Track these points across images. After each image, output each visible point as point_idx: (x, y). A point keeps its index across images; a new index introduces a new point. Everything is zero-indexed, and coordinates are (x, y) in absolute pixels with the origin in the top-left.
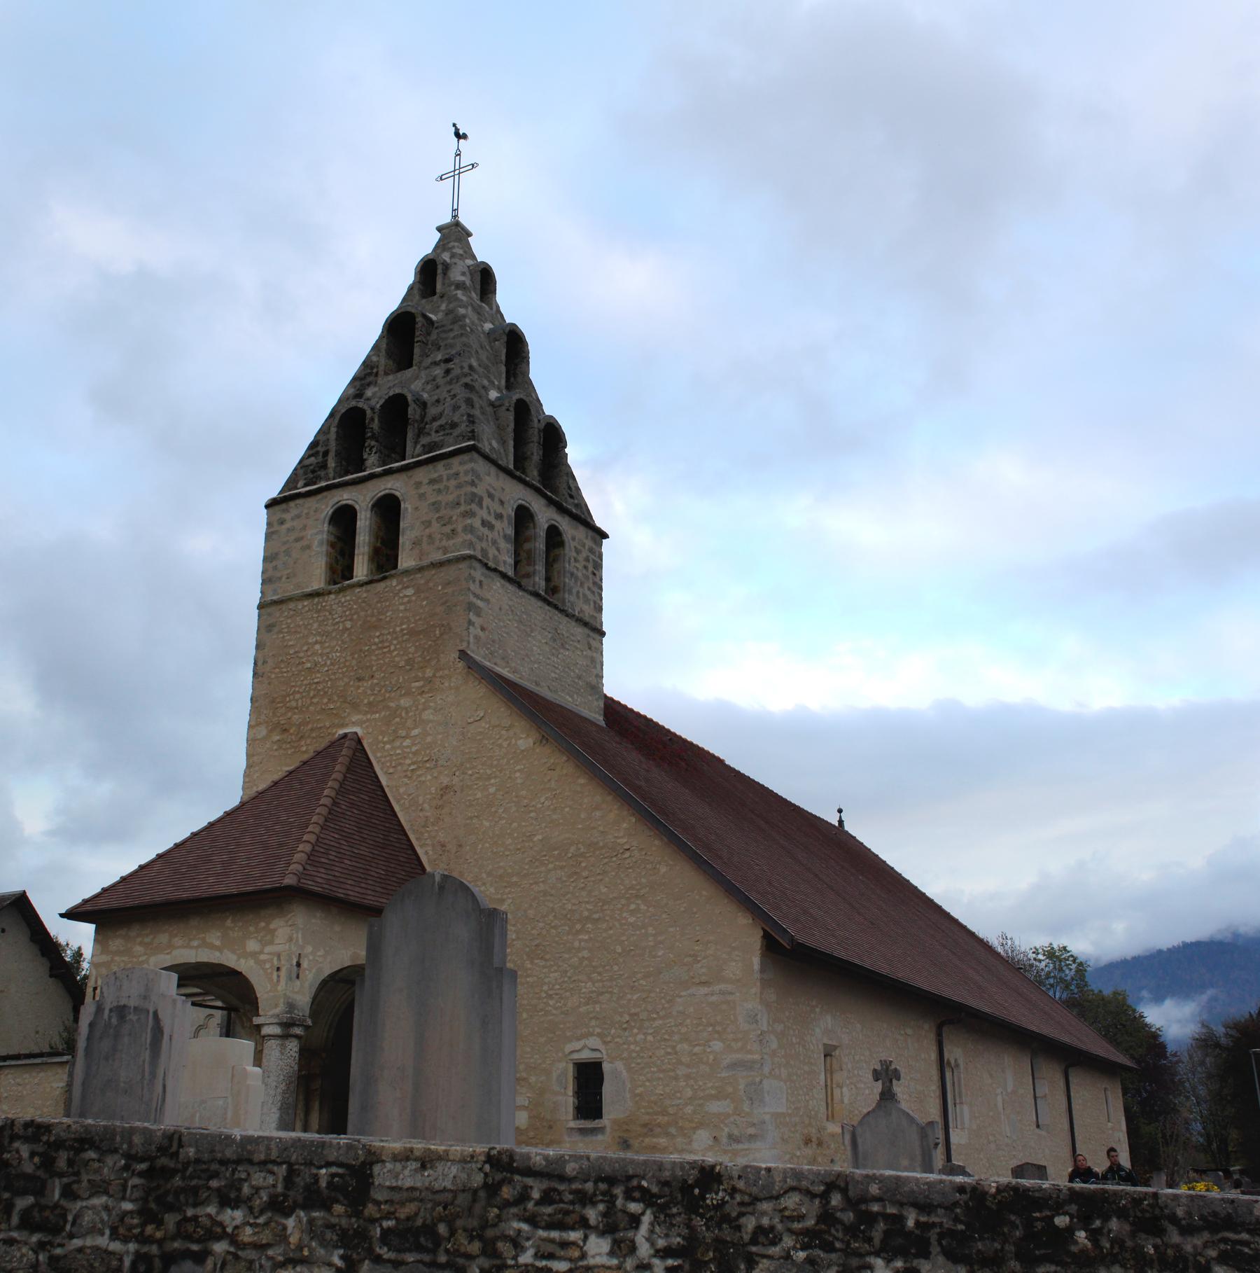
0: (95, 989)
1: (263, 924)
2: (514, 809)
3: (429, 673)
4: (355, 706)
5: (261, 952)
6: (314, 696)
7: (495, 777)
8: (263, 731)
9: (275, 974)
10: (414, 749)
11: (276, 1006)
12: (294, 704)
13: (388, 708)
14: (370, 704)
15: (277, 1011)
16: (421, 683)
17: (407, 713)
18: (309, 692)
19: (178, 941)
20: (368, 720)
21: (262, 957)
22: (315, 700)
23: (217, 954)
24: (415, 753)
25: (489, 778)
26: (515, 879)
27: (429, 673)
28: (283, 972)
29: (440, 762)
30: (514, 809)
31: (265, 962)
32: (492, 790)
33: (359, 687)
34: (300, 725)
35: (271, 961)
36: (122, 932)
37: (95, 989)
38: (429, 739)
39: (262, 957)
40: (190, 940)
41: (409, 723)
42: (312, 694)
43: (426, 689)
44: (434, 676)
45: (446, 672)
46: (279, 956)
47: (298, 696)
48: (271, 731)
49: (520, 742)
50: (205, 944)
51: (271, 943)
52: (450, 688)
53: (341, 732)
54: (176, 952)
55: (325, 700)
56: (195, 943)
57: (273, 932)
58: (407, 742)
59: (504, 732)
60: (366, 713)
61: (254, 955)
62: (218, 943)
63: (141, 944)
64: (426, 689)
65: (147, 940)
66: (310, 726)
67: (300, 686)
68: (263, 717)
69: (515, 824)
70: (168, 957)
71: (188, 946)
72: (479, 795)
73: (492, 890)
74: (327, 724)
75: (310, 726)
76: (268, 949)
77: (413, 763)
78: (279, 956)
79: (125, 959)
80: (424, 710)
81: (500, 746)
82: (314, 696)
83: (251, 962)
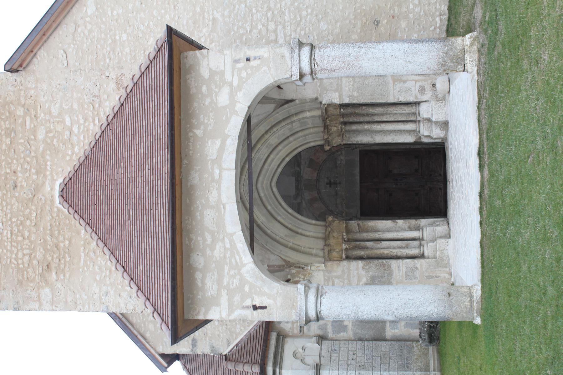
0: (255, 308)
1: (204, 89)
2: (142, 15)
3: (20, 112)
4: (37, 189)
5: (231, 84)
6: (23, 236)
7: (115, 35)
8: (46, 292)
9: (253, 63)
10: (82, 121)
11: (283, 56)
12: (27, 258)
13: (44, 151)
14: (37, 173)
15: (287, 54)
16: (28, 119)
17: (50, 131)
18: (18, 242)
19: (213, 197)
20: (51, 173)
21: (235, 83)
22: (27, 234)
23: (229, 141)
24: (86, 120)
25: (114, 41)
26: (198, 9)
27: (20, 112)
28: (250, 53)
29: (96, 93)
30: (142, 15)
31: (240, 78)
32: (125, 37)
33: (22, 186)
34: (46, 250)
35: (240, 70)
36: (198, 275)
37: (255, 308)
38: (75, 106)
39: (235, 83)
40: (213, 180)
41: (59, 128)
42: (20, 238)
43: (33, 113)
44: (23, 106)
45: (22, 93)
46: (236, 61)
47: (20, 255)
48: (47, 283)
49: (89, 12)
50: (218, 160)
51: (222, 73)
52: (36, 87)
53: (57, 199)
54: (224, 200)
55: (28, 223)
56: (217, 171)
57: (213, 73)
58: (75, 129)
59: (79, 30)
60: (45, 176)
61: (232, 95)
62: (218, 142)
63: (213, 250)
64: (33, 113)
65: (209, 240)
66: (48, 238)
67: (12, 252)
68: (34, 294)
69: (155, 13)
70: (227, 207)
71: (219, 182)
72: (127, 50)
73: (204, 30)
74: (49, 218)
75: (48, 238)
76: (228, 77)
77: (94, 121)
78: (236, 61)
79: (226, 268)
80: (50, 113)
81: (90, 31)
82: (23, 236)
83: (240, 95)
